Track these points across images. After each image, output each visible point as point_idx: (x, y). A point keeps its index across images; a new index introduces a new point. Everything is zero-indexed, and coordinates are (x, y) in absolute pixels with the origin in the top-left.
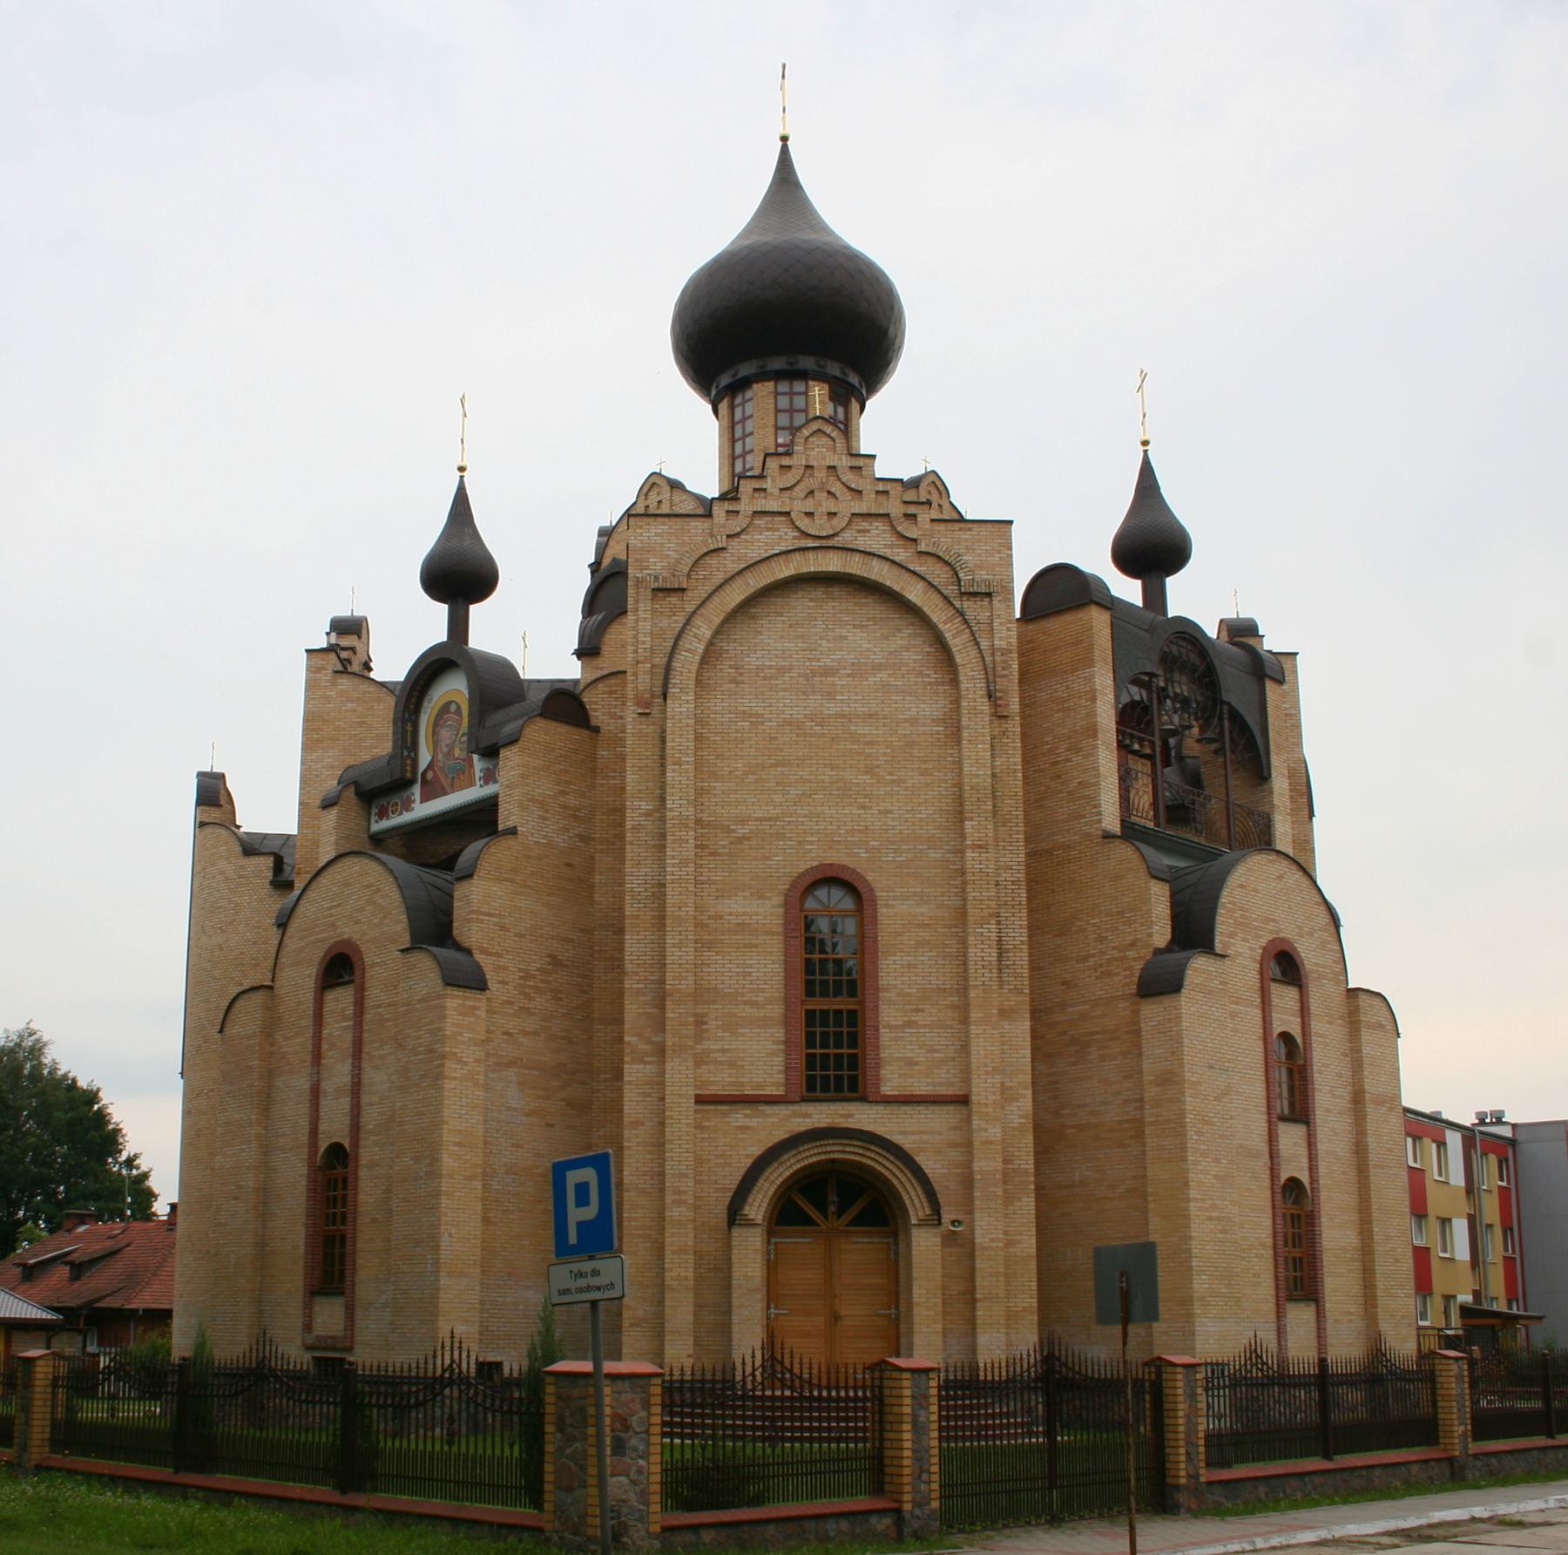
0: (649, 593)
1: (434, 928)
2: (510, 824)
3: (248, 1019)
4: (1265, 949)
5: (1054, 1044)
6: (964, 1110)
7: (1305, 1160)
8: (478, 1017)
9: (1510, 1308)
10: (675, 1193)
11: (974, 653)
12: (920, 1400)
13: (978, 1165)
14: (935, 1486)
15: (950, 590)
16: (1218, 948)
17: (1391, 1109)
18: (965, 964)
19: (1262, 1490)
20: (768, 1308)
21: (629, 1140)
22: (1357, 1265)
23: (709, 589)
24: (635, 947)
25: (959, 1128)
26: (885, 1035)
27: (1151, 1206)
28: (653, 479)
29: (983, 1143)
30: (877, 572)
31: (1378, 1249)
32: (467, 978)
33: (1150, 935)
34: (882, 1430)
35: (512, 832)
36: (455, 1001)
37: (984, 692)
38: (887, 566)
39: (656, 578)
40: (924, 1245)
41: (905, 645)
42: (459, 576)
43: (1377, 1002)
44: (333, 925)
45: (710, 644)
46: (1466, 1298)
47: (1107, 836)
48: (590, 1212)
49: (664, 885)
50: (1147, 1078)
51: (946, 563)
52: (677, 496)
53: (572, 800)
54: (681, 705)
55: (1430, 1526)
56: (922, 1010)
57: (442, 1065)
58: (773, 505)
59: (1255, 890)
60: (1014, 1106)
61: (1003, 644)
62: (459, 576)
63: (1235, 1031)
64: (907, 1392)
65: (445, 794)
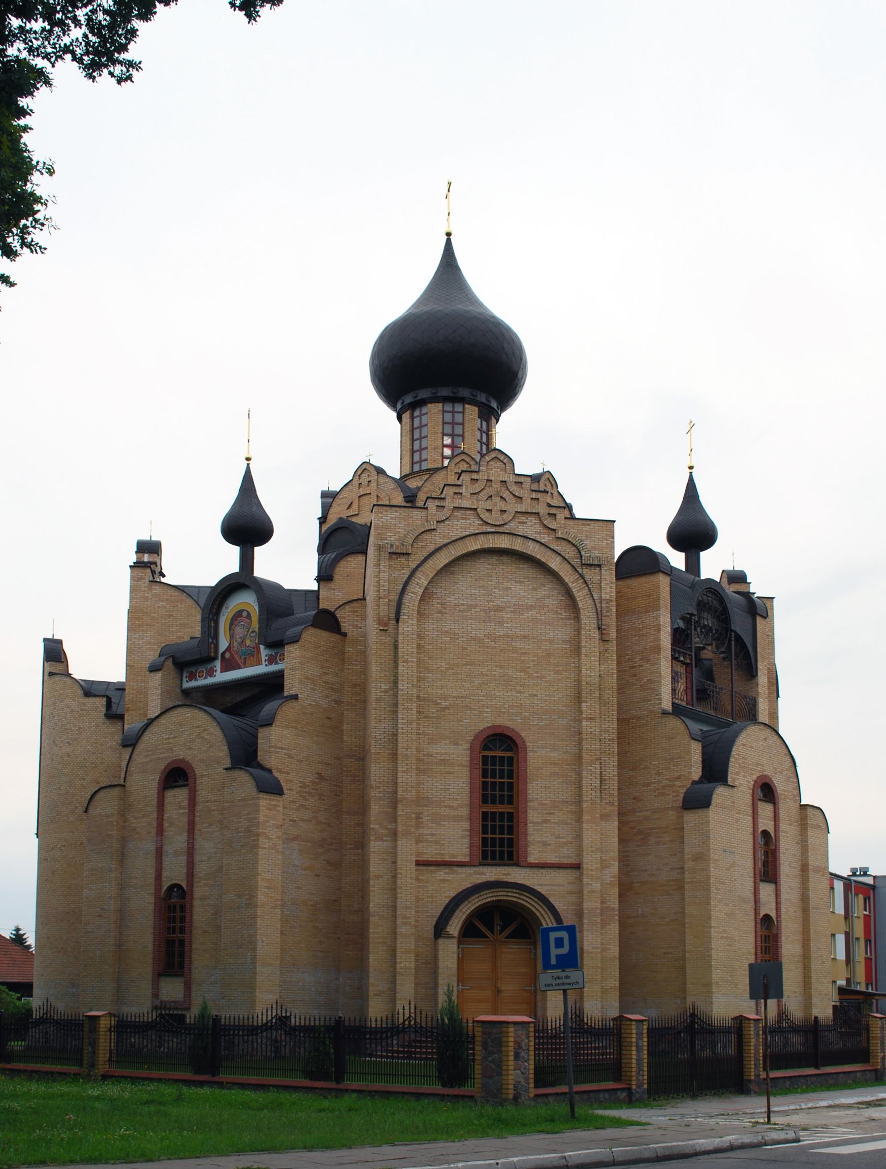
0: (387, 555)
1: (245, 755)
2: (293, 692)
3: (107, 805)
4: (755, 782)
5: (631, 835)
6: (578, 873)
7: (774, 904)
8: (279, 811)
9: (867, 989)
10: (403, 918)
11: (590, 601)
12: (639, 1035)
13: (586, 905)
14: (645, 1077)
15: (576, 562)
16: (729, 783)
17: (823, 875)
18: (580, 787)
19: (788, 1084)
21: (374, 886)
22: (800, 965)
23: (426, 554)
24: (377, 771)
25: (574, 883)
26: (531, 828)
27: (687, 930)
28: (365, 466)
30: (532, 549)
31: (813, 955)
32: (271, 787)
33: (690, 773)
34: (621, 1050)
35: (295, 697)
36: (265, 801)
37: (596, 626)
38: (538, 546)
39: (392, 546)
41: (547, 595)
42: (247, 527)
43: (817, 812)
44: (171, 749)
45: (426, 588)
46: (842, 983)
47: (665, 713)
48: (565, 950)
49: (396, 735)
50: (686, 857)
51: (574, 545)
52: (382, 479)
53: (330, 678)
54: (408, 625)
55: (878, 1100)
56: (553, 814)
57: (258, 840)
58: (466, 504)
59: (751, 747)
60: (607, 871)
61: (608, 597)
62: (247, 527)
63: (738, 829)
64: (634, 1031)
65: (239, 668)
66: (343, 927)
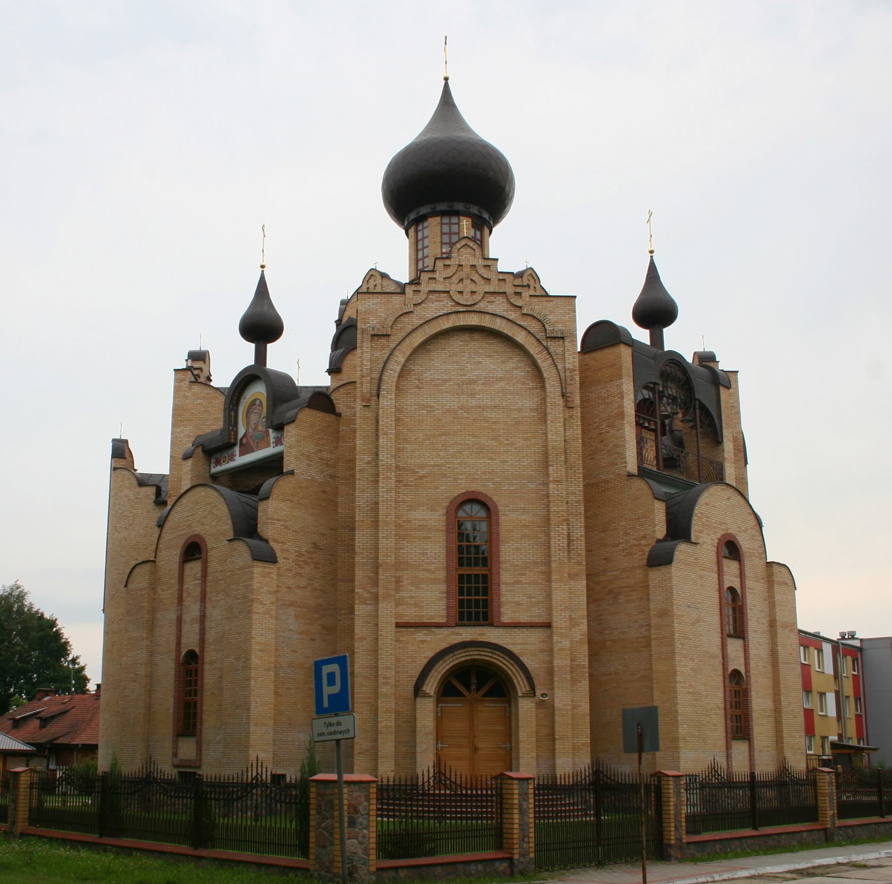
0: (369, 337)
1: (247, 528)
2: (290, 468)
3: (141, 580)
4: (719, 539)
5: (599, 594)
6: (548, 631)
7: (743, 660)
8: (272, 578)
9: (859, 743)
10: (384, 678)
11: (554, 371)
12: (524, 796)
13: (556, 662)
14: (532, 845)
15: (541, 336)
16: (693, 539)
17: (791, 631)
18: (549, 548)
19: (718, 847)
20: (437, 743)
21: (358, 648)
22: (772, 719)
23: (404, 335)
24: (361, 538)
25: (546, 642)
26: (504, 589)
27: (655, 686)
28: (371, 273)
29: (559, 650)
30: (499, 325)
31: (784, 710)
32: (266, 556)
33: (654, 532)
34: (502, 813)
35: (292, 473)
36: (259, 569)
37: (560, 393)
38: (504, 322)
39: (373, 329)
40: (526, 708)
41: (515, 366)
42: (261, 327)
43: (783, 569)
44: (190, 526)
45: (404, 366)
46: (834, 738)
47: (630, 475)
48: (336, 689)
49: (378, 503)
50: (653, 613)
51: (538, 320)
52: (385, 282)
53: (325, 455)
54: (387, 401)
55: (814, 867)
56: (525, 574)
57: (251, 606)
58: (440, 287)
59: (714, 506)
60: (577, 629)
61: (571, 366)
62: (261, 327)
63: (703, 586)
64: (516, 791)
65: (253, 451)
66: (331, 690)
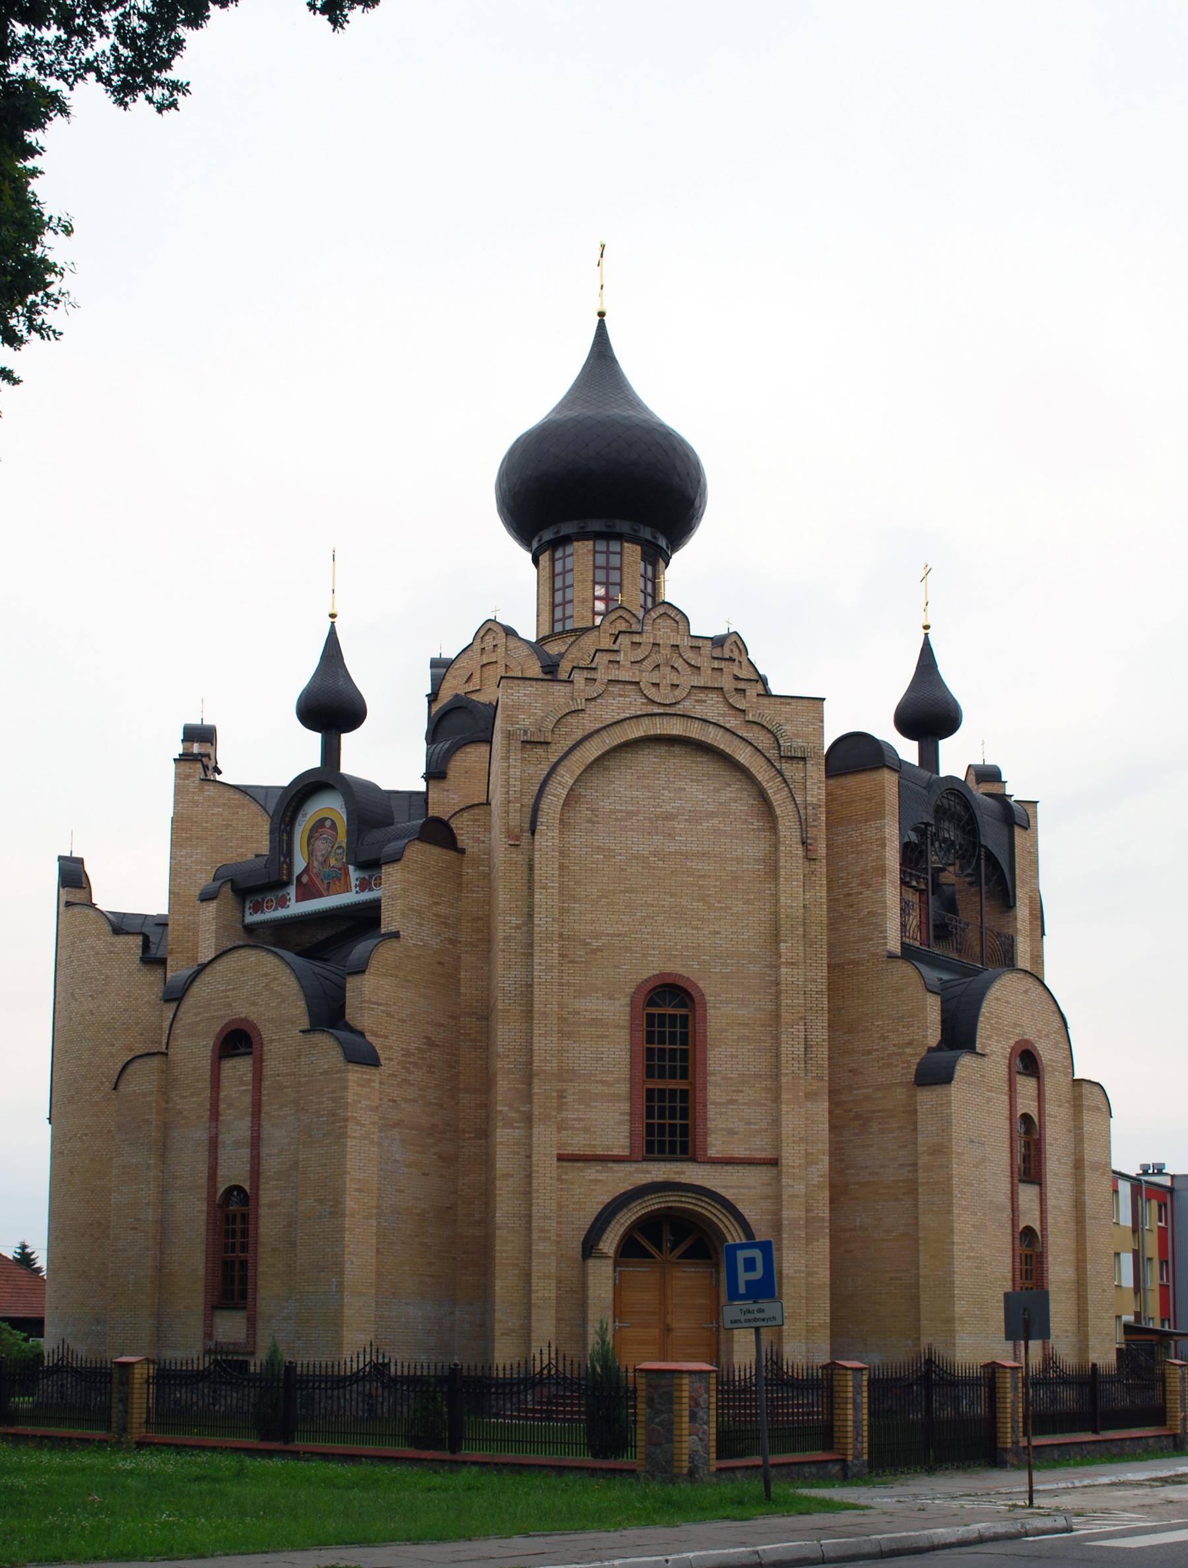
0: (519, 744)
1: (328, 1013)
2: (393, 929)
3: (143, 1079)
4: (1013, 1048)
5: (847, 1119)
6: (774, 1170)
7: (1038, 1213)
8: (374, 1088)
9: (1163, 1326)
10: (540, 1231)
11: (791, 807)
12: (857, 1388)
13: (785, 1214)
14: (866, 1445)
15: (772, 754)
16: (978, 1050)
17: (1103, 1174)
18: (778, 1056)
19: (1056, 1453)
21: (501, 1189)
22: (1073, 1294)
23: (571, 743)
24: (505, 1035)
25: (770, 1184)
26: (711, 1110)
27: (921, 1248)
28: (489, 625)
30: (713, 737)
31: (1091, 1281)
32: (363, 1055)
33: (925, 1037)
34: (832, 1408)
35: (396, 935)
36: (355, 1075)
37: (799, 840)
38: (721, 732)
39: (525, 732)
41: (733, 798)
42: (331, 707)
43: (1096, 1090)
44: (230, 1005)
45: (571, 789)
46: (1129, 1318)
47: (891, 956)
48: (758, 1274)
49: (531, 986)
50: (920, 1149)
51: (769, 731)
52: (512, 643)
53: (443, 910)
54: (547, 839)
55: (1177, 1476)
56: (742, 1091)
57: (346, 1127)
58: (624, 676)
59: (1007, 1002)
60: (813, 1168)
61: (815, 800)
62: (331, 707)
63: (989, 1113)
64: (850, 1383)
65: (321, 896)
